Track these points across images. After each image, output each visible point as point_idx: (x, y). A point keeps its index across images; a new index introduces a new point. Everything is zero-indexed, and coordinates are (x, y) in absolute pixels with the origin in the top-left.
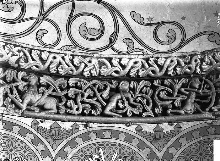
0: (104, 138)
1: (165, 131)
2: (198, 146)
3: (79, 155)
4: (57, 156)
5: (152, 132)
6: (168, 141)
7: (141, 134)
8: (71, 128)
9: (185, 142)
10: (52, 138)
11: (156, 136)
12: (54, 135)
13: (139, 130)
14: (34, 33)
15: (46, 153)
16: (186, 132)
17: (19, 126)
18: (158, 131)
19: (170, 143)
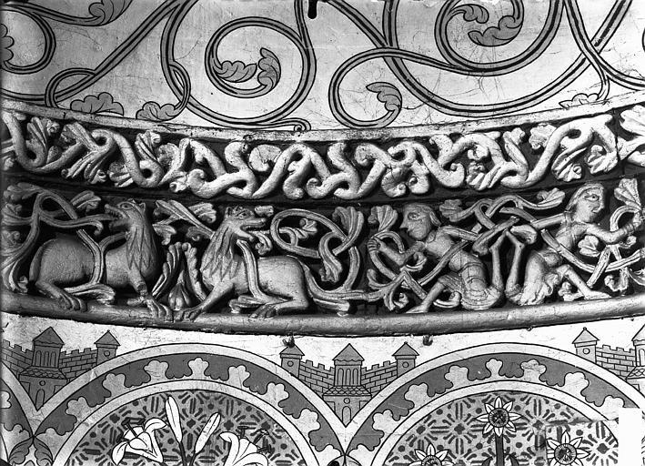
0: (190, 377)
1: (367, 364)
2: (466, 416)
3: (603, 441)
4: (354, 444)
5: (329, 364)
6: (373, 394)
7: (295, 370)
8: (393, 360)
9: (424, 397)
10: (335, 392)
11: (348, 377)
12: (349, 383)
13: (291, 355)
14: (593, 27)
15: (321, 438)
16: (130, 359)
17: (540, 360)
18: (348, 360)
19: (377, 401)
